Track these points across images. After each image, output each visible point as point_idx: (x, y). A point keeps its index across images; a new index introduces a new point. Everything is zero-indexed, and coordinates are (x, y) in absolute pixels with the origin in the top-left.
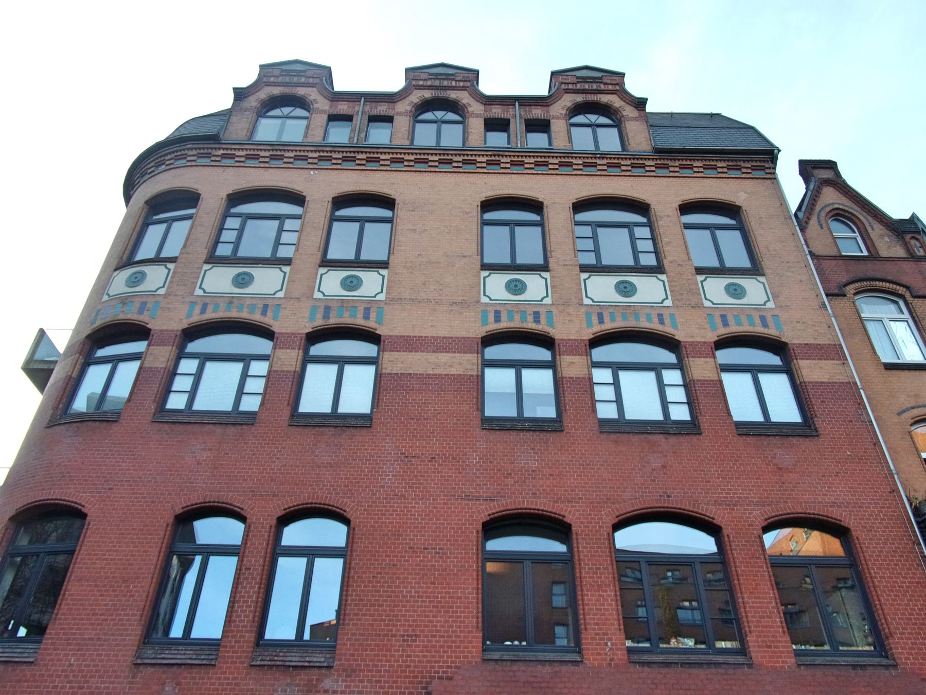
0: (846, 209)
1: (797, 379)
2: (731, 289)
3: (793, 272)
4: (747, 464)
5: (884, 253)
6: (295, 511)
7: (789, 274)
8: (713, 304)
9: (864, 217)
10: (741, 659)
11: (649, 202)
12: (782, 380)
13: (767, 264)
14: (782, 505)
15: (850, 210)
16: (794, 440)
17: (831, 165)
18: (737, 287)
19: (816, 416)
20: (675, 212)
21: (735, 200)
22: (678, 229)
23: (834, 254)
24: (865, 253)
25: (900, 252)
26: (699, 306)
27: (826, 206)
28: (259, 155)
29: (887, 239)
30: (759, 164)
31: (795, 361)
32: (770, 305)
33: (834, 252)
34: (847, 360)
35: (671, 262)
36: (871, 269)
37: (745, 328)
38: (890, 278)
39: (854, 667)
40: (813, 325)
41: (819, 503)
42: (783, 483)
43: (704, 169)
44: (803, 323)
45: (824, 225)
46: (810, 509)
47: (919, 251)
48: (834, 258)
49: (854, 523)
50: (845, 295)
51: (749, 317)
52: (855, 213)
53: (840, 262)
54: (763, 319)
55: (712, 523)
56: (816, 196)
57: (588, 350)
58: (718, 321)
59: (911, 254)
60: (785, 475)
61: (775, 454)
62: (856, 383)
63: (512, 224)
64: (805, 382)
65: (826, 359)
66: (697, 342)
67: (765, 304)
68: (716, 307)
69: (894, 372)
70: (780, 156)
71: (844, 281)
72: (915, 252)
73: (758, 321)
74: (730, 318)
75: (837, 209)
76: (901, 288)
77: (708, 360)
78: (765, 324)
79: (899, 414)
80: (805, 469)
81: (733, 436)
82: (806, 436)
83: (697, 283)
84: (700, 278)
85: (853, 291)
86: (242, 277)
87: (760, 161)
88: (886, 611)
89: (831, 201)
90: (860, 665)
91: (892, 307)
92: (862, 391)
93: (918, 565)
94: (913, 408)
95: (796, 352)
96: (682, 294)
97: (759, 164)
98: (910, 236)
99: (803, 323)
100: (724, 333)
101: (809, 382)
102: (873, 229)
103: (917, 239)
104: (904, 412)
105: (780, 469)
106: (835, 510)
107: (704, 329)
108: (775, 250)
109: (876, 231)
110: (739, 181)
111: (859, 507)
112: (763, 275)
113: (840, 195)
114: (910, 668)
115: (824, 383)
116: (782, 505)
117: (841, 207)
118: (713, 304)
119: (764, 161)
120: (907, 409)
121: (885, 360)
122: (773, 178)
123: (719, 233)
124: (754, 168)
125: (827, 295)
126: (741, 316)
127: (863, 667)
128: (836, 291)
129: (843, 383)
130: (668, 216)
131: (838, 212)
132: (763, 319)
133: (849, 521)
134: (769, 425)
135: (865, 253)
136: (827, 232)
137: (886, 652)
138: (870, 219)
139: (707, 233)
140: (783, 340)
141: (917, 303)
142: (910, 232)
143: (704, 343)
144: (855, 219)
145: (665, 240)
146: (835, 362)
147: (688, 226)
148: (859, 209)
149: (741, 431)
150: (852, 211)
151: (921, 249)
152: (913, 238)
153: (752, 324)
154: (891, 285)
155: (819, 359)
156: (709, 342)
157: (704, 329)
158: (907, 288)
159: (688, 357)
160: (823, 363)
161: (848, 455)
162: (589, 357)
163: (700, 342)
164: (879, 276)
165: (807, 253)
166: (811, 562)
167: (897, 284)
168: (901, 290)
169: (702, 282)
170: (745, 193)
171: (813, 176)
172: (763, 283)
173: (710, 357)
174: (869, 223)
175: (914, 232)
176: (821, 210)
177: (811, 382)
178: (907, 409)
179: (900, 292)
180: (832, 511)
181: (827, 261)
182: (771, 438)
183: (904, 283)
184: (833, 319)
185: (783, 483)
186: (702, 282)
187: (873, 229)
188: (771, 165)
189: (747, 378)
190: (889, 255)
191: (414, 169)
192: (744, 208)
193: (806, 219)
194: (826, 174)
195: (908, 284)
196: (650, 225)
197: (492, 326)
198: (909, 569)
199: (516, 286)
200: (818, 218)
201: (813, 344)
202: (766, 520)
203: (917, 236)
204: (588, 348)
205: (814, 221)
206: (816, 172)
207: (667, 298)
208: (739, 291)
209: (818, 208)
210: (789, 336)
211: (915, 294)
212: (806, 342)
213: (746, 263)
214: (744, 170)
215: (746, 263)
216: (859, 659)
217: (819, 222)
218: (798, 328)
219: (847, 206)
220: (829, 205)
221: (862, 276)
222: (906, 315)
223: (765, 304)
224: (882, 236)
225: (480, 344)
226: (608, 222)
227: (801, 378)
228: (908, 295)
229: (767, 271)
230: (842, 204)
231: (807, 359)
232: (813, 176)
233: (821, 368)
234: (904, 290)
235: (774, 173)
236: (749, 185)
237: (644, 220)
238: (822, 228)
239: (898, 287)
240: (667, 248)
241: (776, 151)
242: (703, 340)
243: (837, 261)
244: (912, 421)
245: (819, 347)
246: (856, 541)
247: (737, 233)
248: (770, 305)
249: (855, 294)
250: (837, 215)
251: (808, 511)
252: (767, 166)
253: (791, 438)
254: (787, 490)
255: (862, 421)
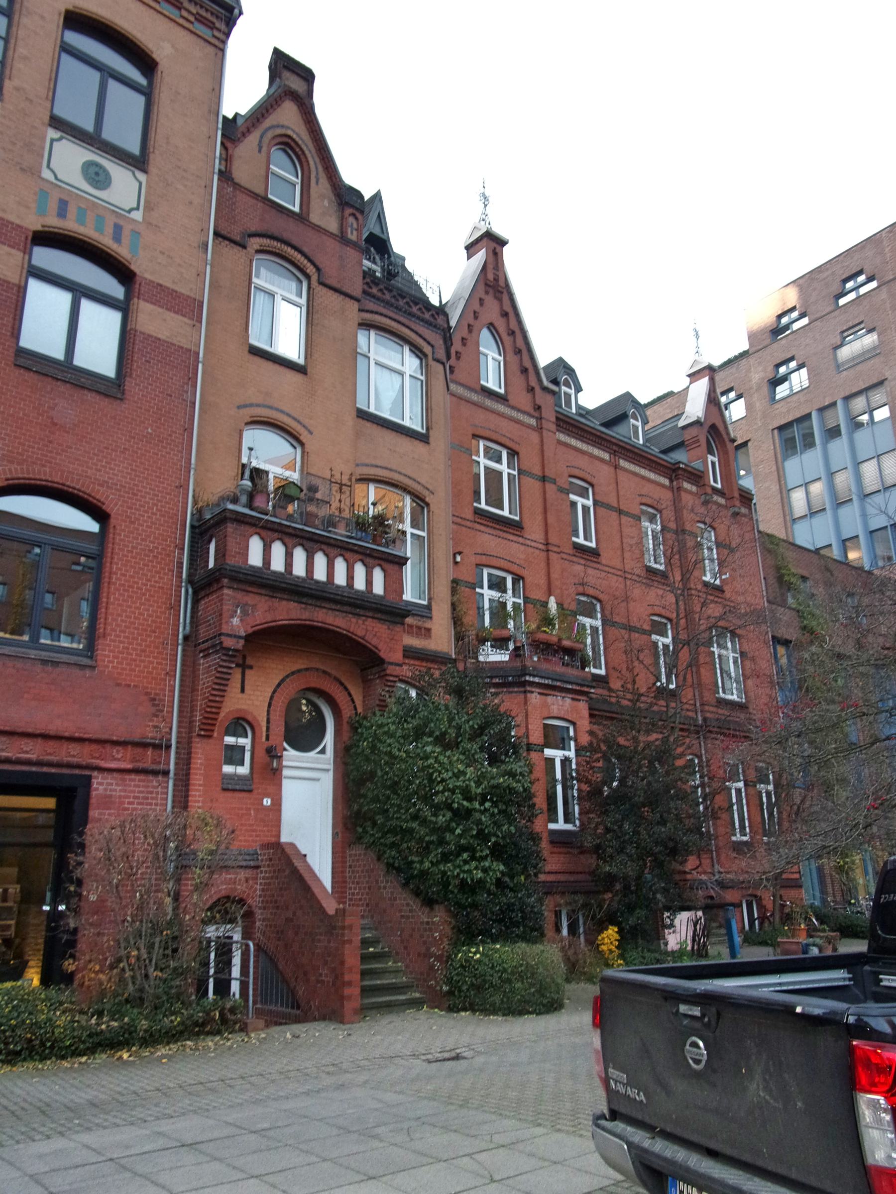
0: (300, 142)
1: (129, 324)
2: (93, 170)
3: (186, 186)
4: (10, 406)
5: (314, 218)
6: (78, 496)
7: (179, 186)
8: (56, 178)
9: (315, 164)
10: (86, 661)
11: (158, 59)
12: (112, 319)
13: (156, 160)
14: (36, 468)
15: (303, 146)
16: (89, 396)
17: (307, 76)
18: (101, 172)
19: (131, 376)
20: (56, 17)
21: (154, 49)
22: (49, 46)
23: (257, 191)
24: (297, 209)
25: (332, 225)
26: (35, 172)
27: (278, 126)
28: (214, 24)
29: (326, 203)
30: (208, 16)
31: (136, 300)
32: (138, 216)
33: (259, 190)
34: (201, 322)
35: (17, 89)
36: (290, 229)
37: (87, 230)
38: (305, 249)
39: (44, 662)
40: (179, 265)
41: (87, 477)
42: (50, 442)
43: (196, 19)
44: (169, 256)
45: (264, 149)
46: (72, 481)
47: (352, 233)
48: (255, 196)
49: (118, 509)
50: (244, 247)
51: (100, 219)
52: (307, 152)
53: (260, 204)
54: (118, 229)
55: (100, 509)
56: (272, 107)
57: (28, 246)
58: (53, 205)
59: (342, 233)
60: (57, 433)
61: (56, 405)
62: (198, 354)
63: (108, 73)
64: (136, 331)
65: (176, 313)
66: (8, 222)
67: (129, 211)
68: (57, 184)
69: (257, 360)
70: (239, 22)
71: (253, 229)
72: (346, 232)
73: (109, 230)
74: (72, 211)
75: (289, 137)
76: (312, 267)
77: (13, 251)
78: (117, 238)
79: (239, 407)
80: (87, 433)
81: (6, 364)
82: (106, 396)
83: (44, 138)
84: (52, 134)
85: (256, 247)
86: (97, 169)
87: (212, 14)
88: (110, 611)
89: (286, 123)
90: (52, 661)
91: (294, 285)
92: (200, 366)
93: (169, 570)
94: (258, 405)
95: (142, 289)
96: (14, 144)
97: (208, 16)
98: (350, 211)
99: (169, 256)
100: (54, 225)
101: (141, 332)
102: (317, 183)
103: (357, 219)
104: (245, 406)
105: (55, 424)
106: (102, 490)
107: (28, 207)
108: (176, 147)
109: (321, 188)
110: (172, 25)
111: (134, 494)
112: (145, 171)
113: (301, 122)
114: (109, 672)
115: (159, 339)
116: (36, 468)
117: (295, 136)
118: (56, 178)
119: (217, 17)
120: (251, 405)
121: (253, 341)
122: (220, 48)
123: (112, 84)
124: (200, 19)
125: (217, 234)
126: (89, 212)
127: (56, 664)
128: (238, 238)
129: (182, 348)
130: (42, 17)
131: (290, 141)
132: (118, 229)
133: (113, 506)
134: (69, 368)
135: (297, 209)
136: (265, 160)
137: (92, 652)
138: (320, 169)
139: (96, 76)
140: (133, 267)
141: (320, 291)
142: (352, 206)
143: (19, 226)
144: (302, 157)
145: (21, 50)
146: (186, 320)
147: (66, 49)
148: (313, 150)
149: (21, 361)
150: (305, 148)
151: (355, 233)
152: (353, 215)
153: (99, 229)
154: (299, 256)
155: (168, 309)
156: (26, 229)
157: (28, 207)
158: (318, 269)
159: (138, 298)
160: (169, 315)
161: (148, 433)
162: (27, 257)
163: (12, 223)
164: (295, 241)
165: (216, 171)
166: (46, 541)
167: (310, 260)
168: (310, 269)
169: (52, 141)
170: (173, 46)
171: (280, 77)
172: (140, 184)
173: (19, 249)
174: (317, 174)
175: (357, 209)
176: (272, 127)
177: (144, 334)
178: (251, 405)
179: (308, 271)
180: (98, 491)
181: (244, 196)
182: (59, 383)
183: (318, 263)
184: (208, 267)
185: (50, 442)
186: (52, 141)
187: (317, 183)
188: (223, 27)
189: (64, 298)
190: (318, 223)
191: (194, 30)
192: (160, 68)
193: (245, 130)
194: (296, 84)
195: (321, 266)
196: (148, 94)
197: (53, 222)
198: (157, 572)
199: (97, 174)
200: (261, 137)
201: (168, 288)
202: (7, 479)
203: (358, 215)
204: (29, 241)
205: (253, 139)
206: (286, 74)
207: (138, 209)
208: (102, 177)
209: (267, 123)
210: (140, 265)
211: (323, 280)
212: (161, 282)
213: (133, 147)
214: (185, 14)
215: (133, 147)
216: (55, 655)
217: (260, 141)
218: (159, 260)
219: (301, 139)
220: (283, 126)
221: (276, 234)
222: (303, 301)
223: (129, 211)
224: (322, 197)
225: (30, 238)
226: (96, 60)
227: (134, 323)
228: (314, 278)
229: (152, 169)
230: (297, 134)
231: (152, 303)
232: (280, 77)
233: (165, 320)
234: (314, 270)
235: (224, 42)
236: (183, 38)
237: (143, 81)
238: (260, 151)
239: (309, 264)
240: (18, 65)
241: (236, 11)
242: (18, 222)
243: (254, 201)
244: (250, 420)
245: (174, 295)
246: (111, 530)
247: (141, 100)
248: (138, 216)
249: (258, 251)
250: (286, 144)
251: (68, 483)
252: (218, 25)
253: (86, 392)
254: (51, 452)
255: (184, 400)
